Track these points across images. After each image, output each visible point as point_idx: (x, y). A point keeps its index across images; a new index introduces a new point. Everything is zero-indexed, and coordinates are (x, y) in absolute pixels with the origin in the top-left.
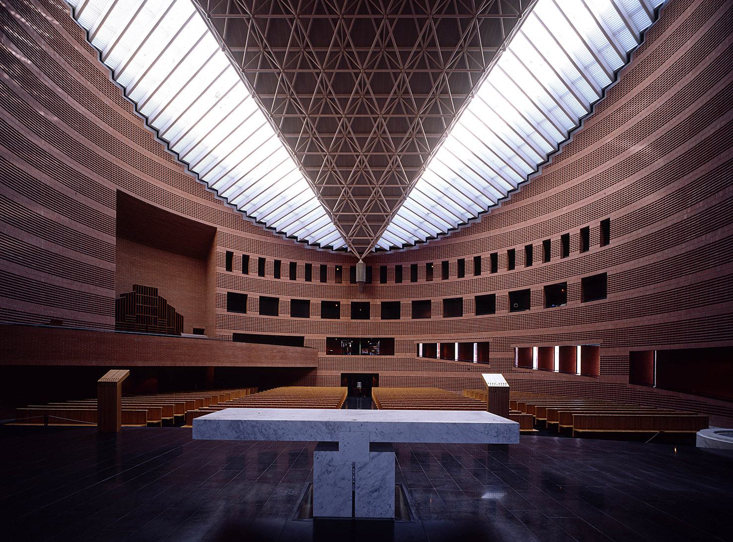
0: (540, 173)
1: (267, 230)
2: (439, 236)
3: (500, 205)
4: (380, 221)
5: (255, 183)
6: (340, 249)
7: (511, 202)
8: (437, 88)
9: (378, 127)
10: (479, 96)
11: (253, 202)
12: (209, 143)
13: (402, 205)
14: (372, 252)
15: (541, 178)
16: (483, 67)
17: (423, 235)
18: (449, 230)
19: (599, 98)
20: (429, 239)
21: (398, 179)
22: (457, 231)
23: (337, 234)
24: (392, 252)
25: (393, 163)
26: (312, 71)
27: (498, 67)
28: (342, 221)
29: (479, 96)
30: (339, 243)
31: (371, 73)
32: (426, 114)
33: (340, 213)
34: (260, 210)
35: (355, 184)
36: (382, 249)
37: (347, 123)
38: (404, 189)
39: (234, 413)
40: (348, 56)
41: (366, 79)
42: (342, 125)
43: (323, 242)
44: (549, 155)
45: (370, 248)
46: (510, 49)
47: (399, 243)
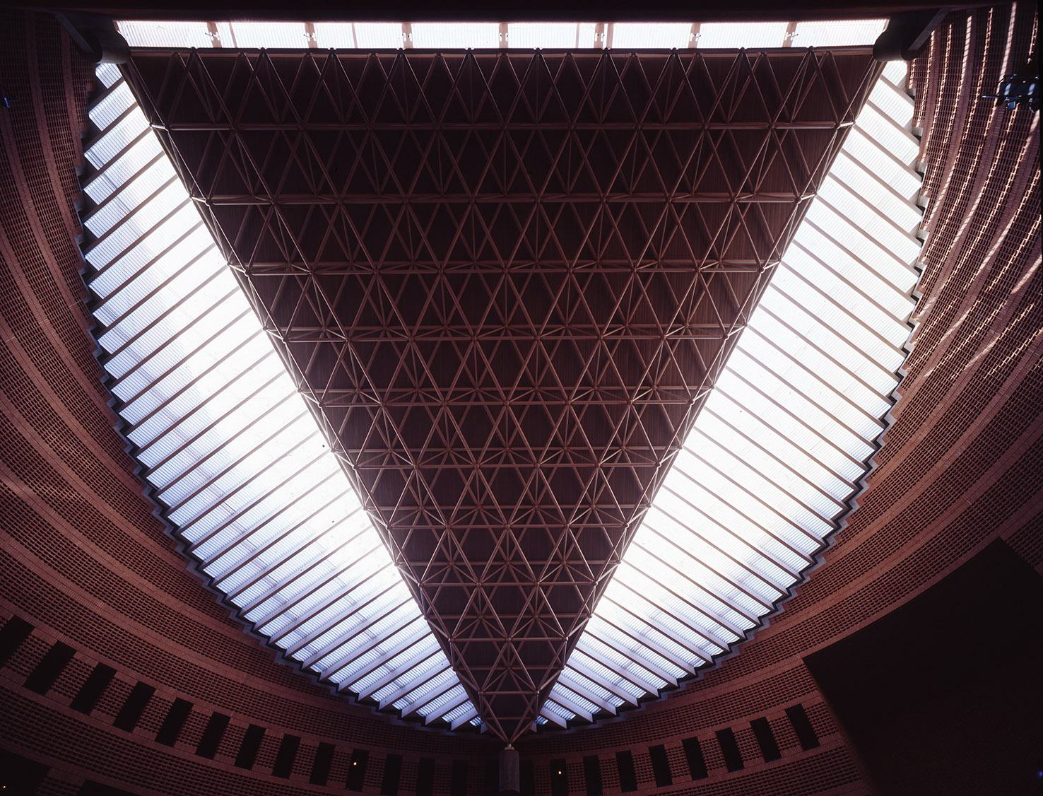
2: (662, 694)
12: (212, 411)
14: (530, 732)
16: (622, 520)
17: (634, 694)
18: (679, 680)
19: (864, 471)
20: (645, 702)
21: (542, 628)
23: (460, 693)
24: (573, 730)
27: (674, 470)
31: (466, 529)
32: (616, 463)
33: (471, 639)
35: (651, 273)
36: (552, 725)
37: (455, 541)
39: (807, 331)
40: (492, 330)
41: (455, 541)
42: (473, 486)
44: (814, 555)
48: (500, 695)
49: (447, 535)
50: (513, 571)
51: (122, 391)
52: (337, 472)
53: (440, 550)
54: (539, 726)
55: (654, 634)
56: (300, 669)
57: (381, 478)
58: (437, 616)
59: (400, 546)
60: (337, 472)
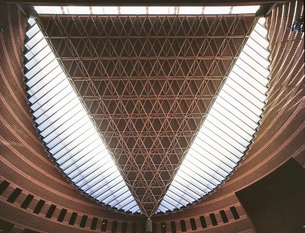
0: (240, 165)
1: (77, 192)
3: (224, 183)
4: (160, 193)
5: (40, 116)
6: (136, 213)
7: (229, 181)
8: (191, 109)
9: (156, 176)
10: (248, 45)
11: (117, 199)
13: (162, 199)
15: (242, 167)
17: (185, 203)
22: (179, 211)
25: (164, 161)
26: (132, 114)
28: (138, 193)
29: (248, 45)
30: (136, 209)
34: (121, 204)
36: (161, 213)
38: (171, 173)
43: (126, 209)
45: (154, 211)
46: (259, 23)
47: (172, 208)
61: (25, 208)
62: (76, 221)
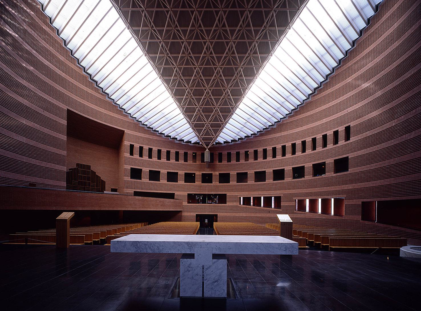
0: (310, 99)
1: (153, 132)
2: (252, 135)
3: (287, 118)
4: (218, 127)
5: (147, 105)
6: (196, 143)
7: (293, 116)
8: (251, 51)
9: (217, 73)
10: (275, 55)
13: (231, 118)
14: (213, 144)
15: (311, 102)
17: (243, 135)
19: (344, 56)
20: (246, 137)
22: (262, 132)
23: (193, 134)
24: (225, 144)
25: (225, 94)
26: (179, 40)
28: (197, 127)
29: (275, 55)
30: (194, 140)
33: (195, 122)
36: (219, 143)
38: (232, 108)
39: (134, 237)
40: (200, 32)
43: (186, 139)
44: (315, 89)
45: (213, 142)
46: (293, 28)
47: (229, 139)
48: (196, 123)
49: (177, 70)
50: (201, 17)
51: (57, 24)
52: (162, 84)
53: (175, 73)
54: (216, 143)
55: (303, 85)
56: (147, 128)
57: (163, 69)
58: (194, 128)
59: (173, 93)
60: (162, 84)
61: (305, 152)
62: (328, 142)
